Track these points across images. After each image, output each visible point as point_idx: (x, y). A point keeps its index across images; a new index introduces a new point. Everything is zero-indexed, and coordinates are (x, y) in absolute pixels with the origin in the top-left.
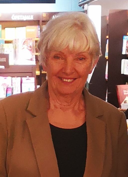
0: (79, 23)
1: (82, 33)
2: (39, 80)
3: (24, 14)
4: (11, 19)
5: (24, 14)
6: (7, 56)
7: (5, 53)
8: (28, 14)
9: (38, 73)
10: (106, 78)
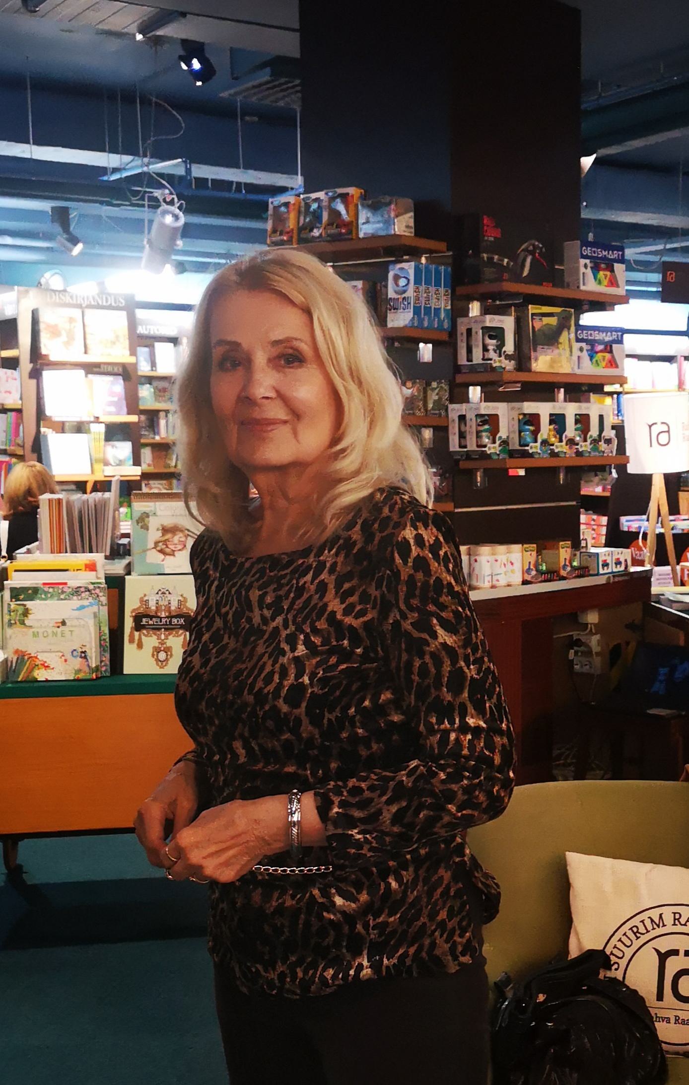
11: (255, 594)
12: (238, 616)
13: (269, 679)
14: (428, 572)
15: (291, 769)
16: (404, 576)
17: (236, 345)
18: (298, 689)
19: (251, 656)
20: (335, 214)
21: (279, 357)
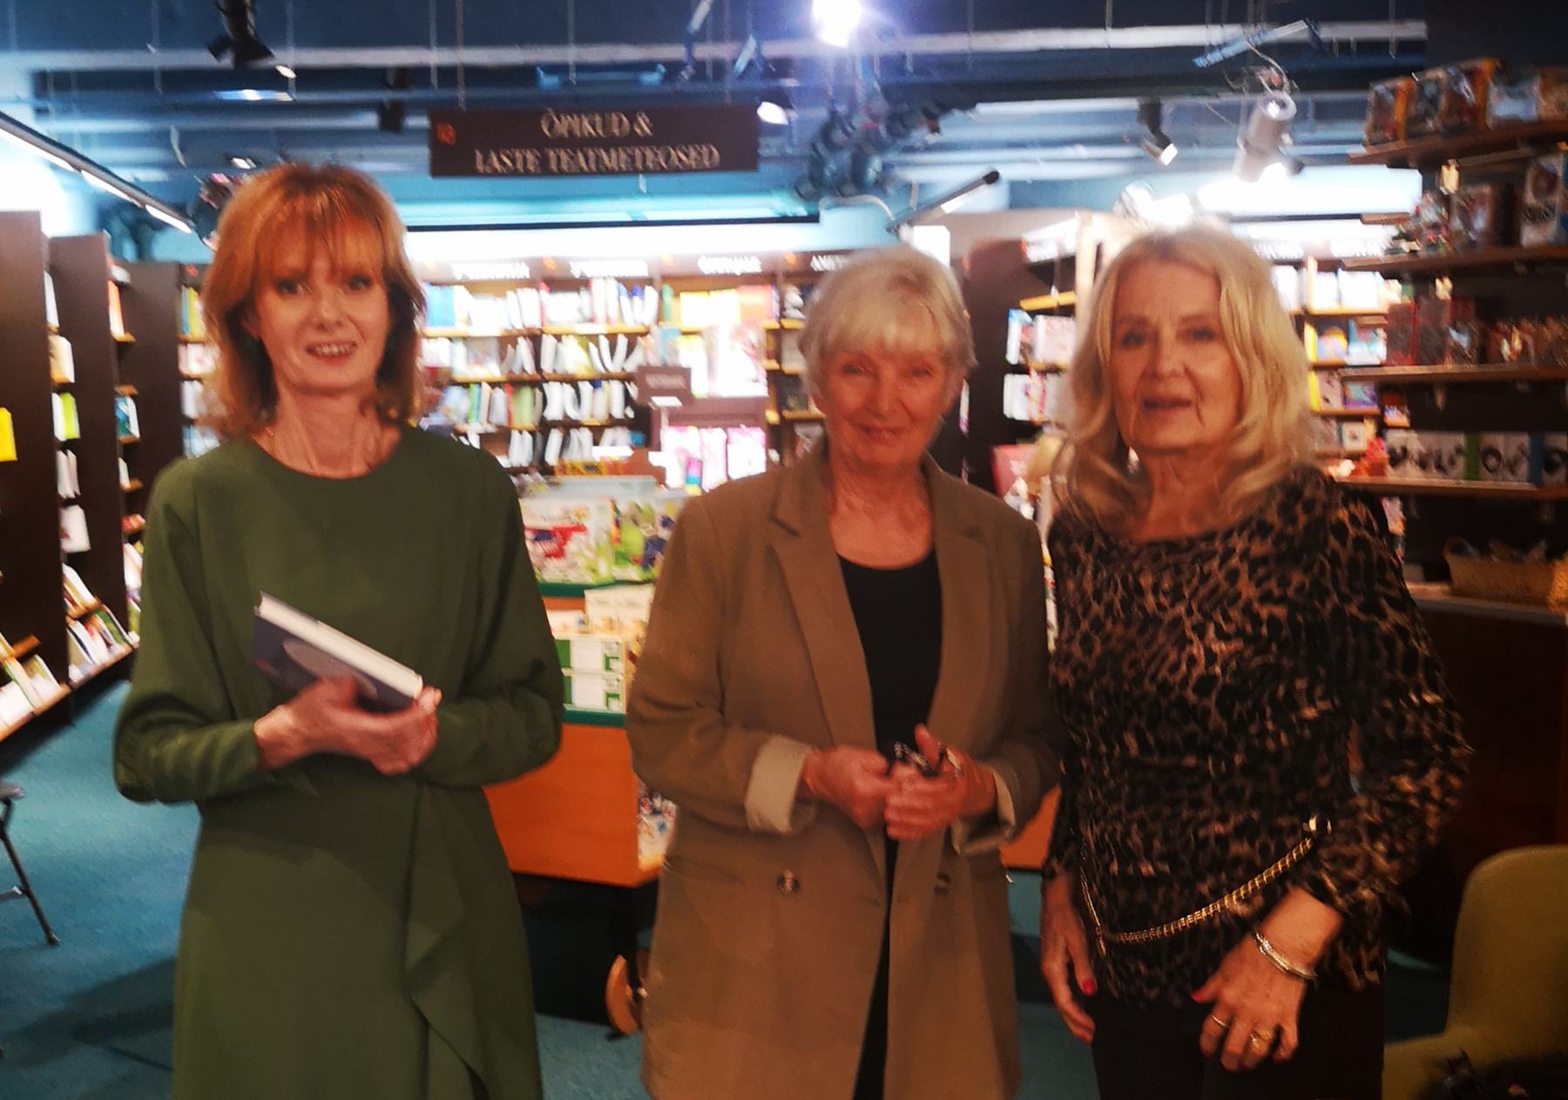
0: (911, 277)
1: (920, 302)
2: (779, 437)
3: (731, 256)
4: (217, 372)
5: (731, 256)
6: (685, 373)
7: (684, 364)
8: (742, 256)
9: (772, 416)
10: (964, 428)
11: (1146, 581)
12: (1126, 604)
13: (1175, 668)
14: (1368, 551)
15: (1190, 761)
16: (1344, 559)
17: (1143, 321)
18: (1206, 683)
19: (1148, 645)
20: (1457, 98)
21: (1189, 331)
